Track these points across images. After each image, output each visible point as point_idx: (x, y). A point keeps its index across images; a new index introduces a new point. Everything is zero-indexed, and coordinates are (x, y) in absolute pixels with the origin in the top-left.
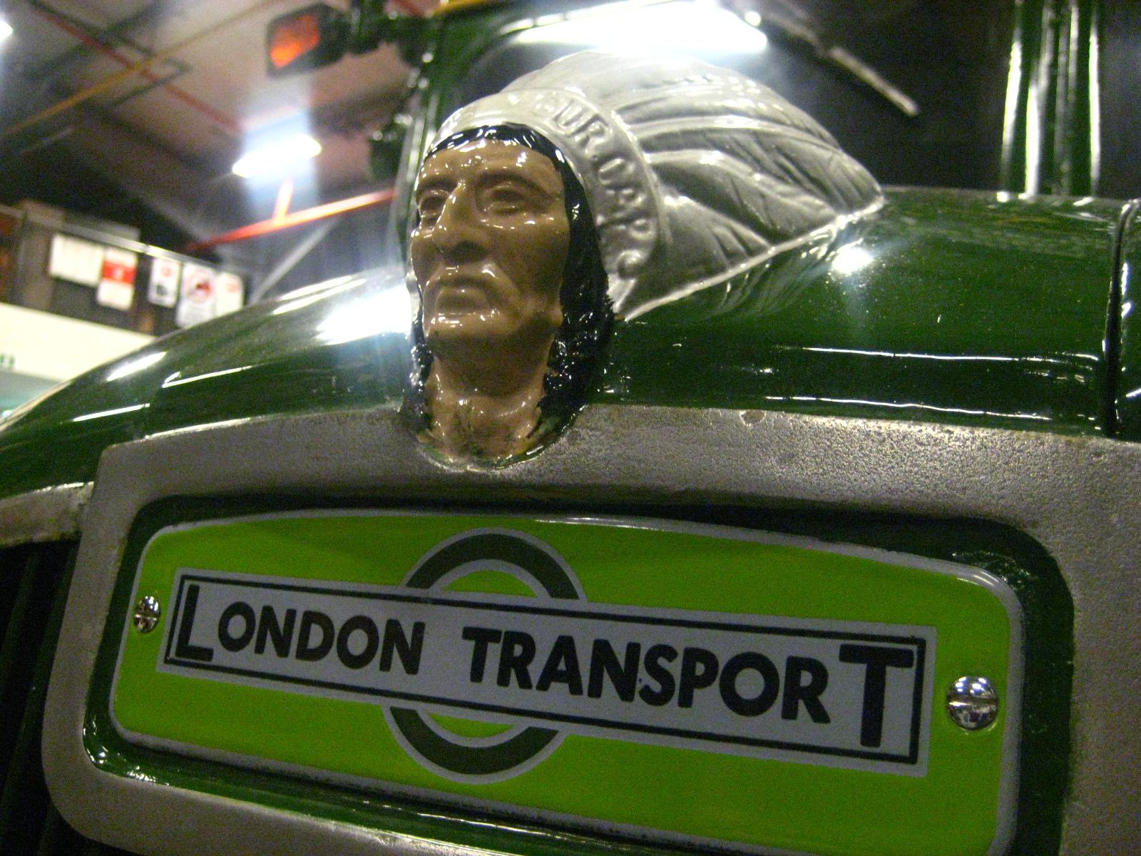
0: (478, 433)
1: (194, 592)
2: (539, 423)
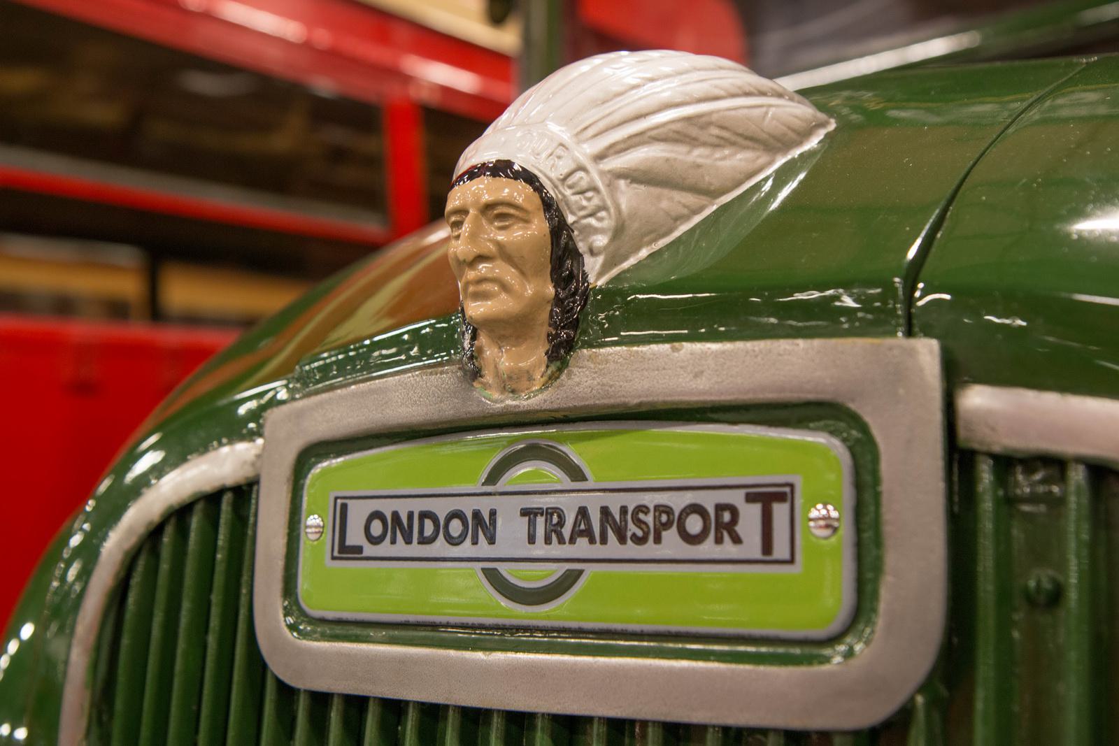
0: (510, 378)
1: (344, 507)
2: (547, 367)
